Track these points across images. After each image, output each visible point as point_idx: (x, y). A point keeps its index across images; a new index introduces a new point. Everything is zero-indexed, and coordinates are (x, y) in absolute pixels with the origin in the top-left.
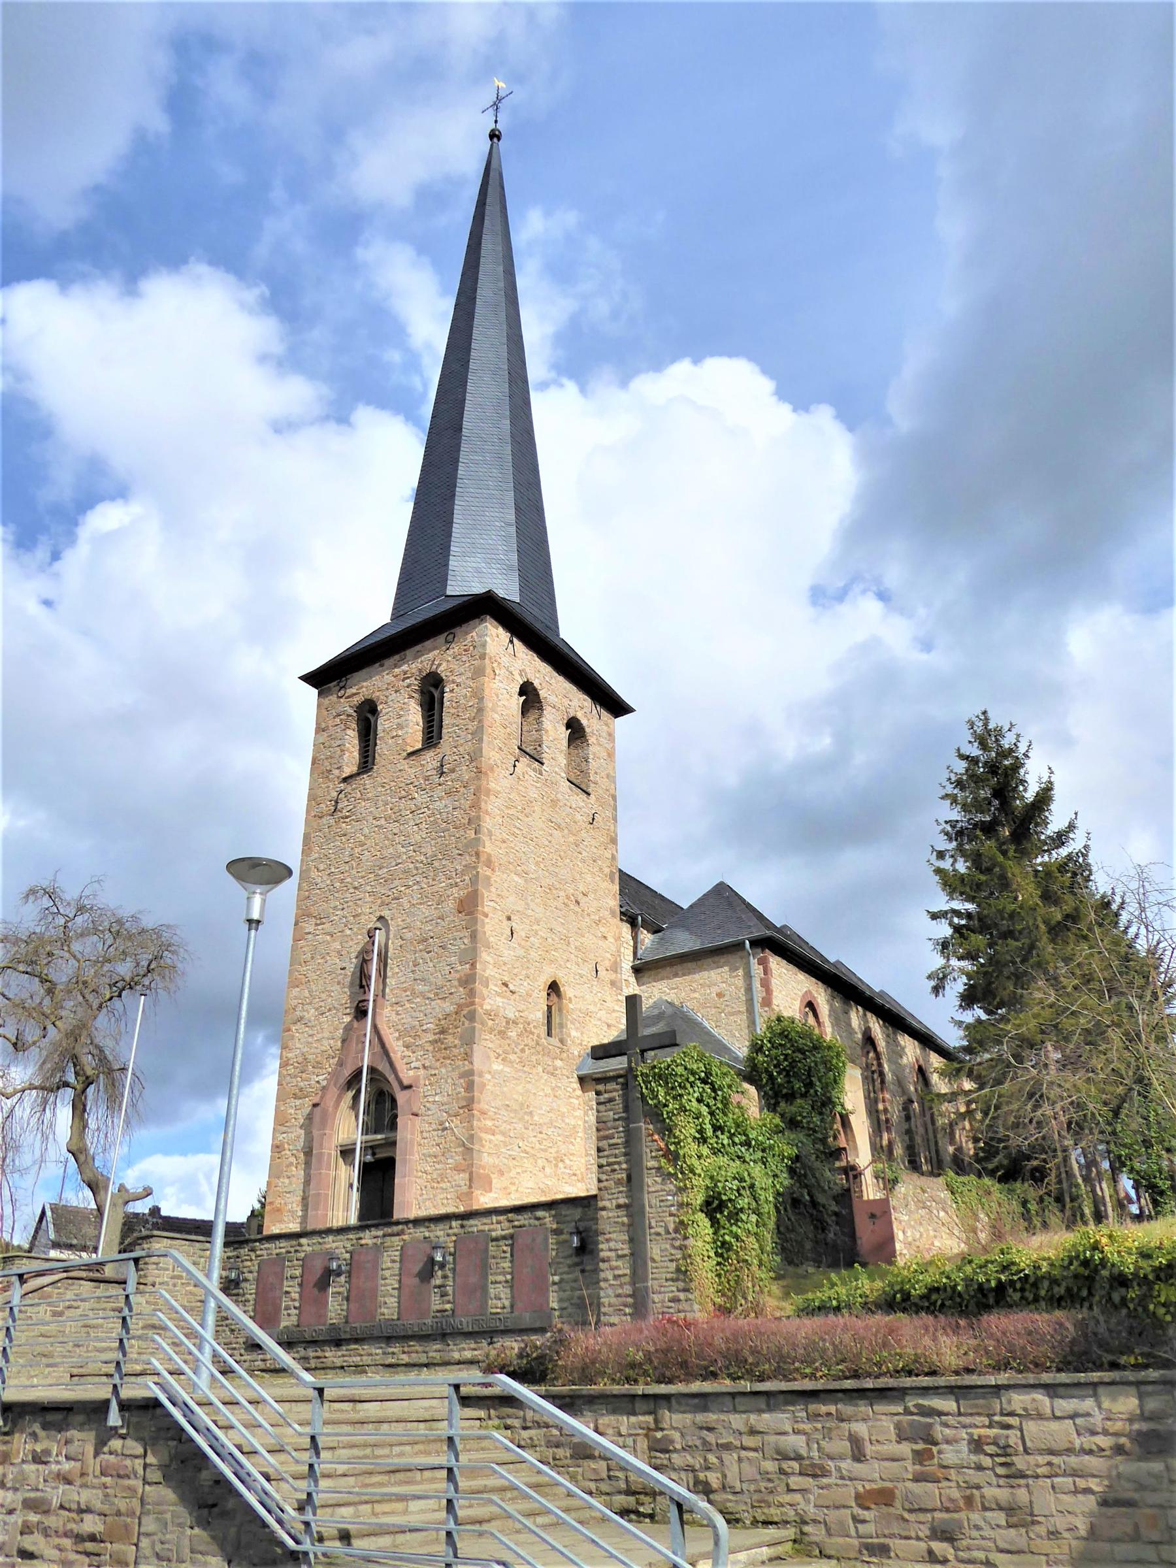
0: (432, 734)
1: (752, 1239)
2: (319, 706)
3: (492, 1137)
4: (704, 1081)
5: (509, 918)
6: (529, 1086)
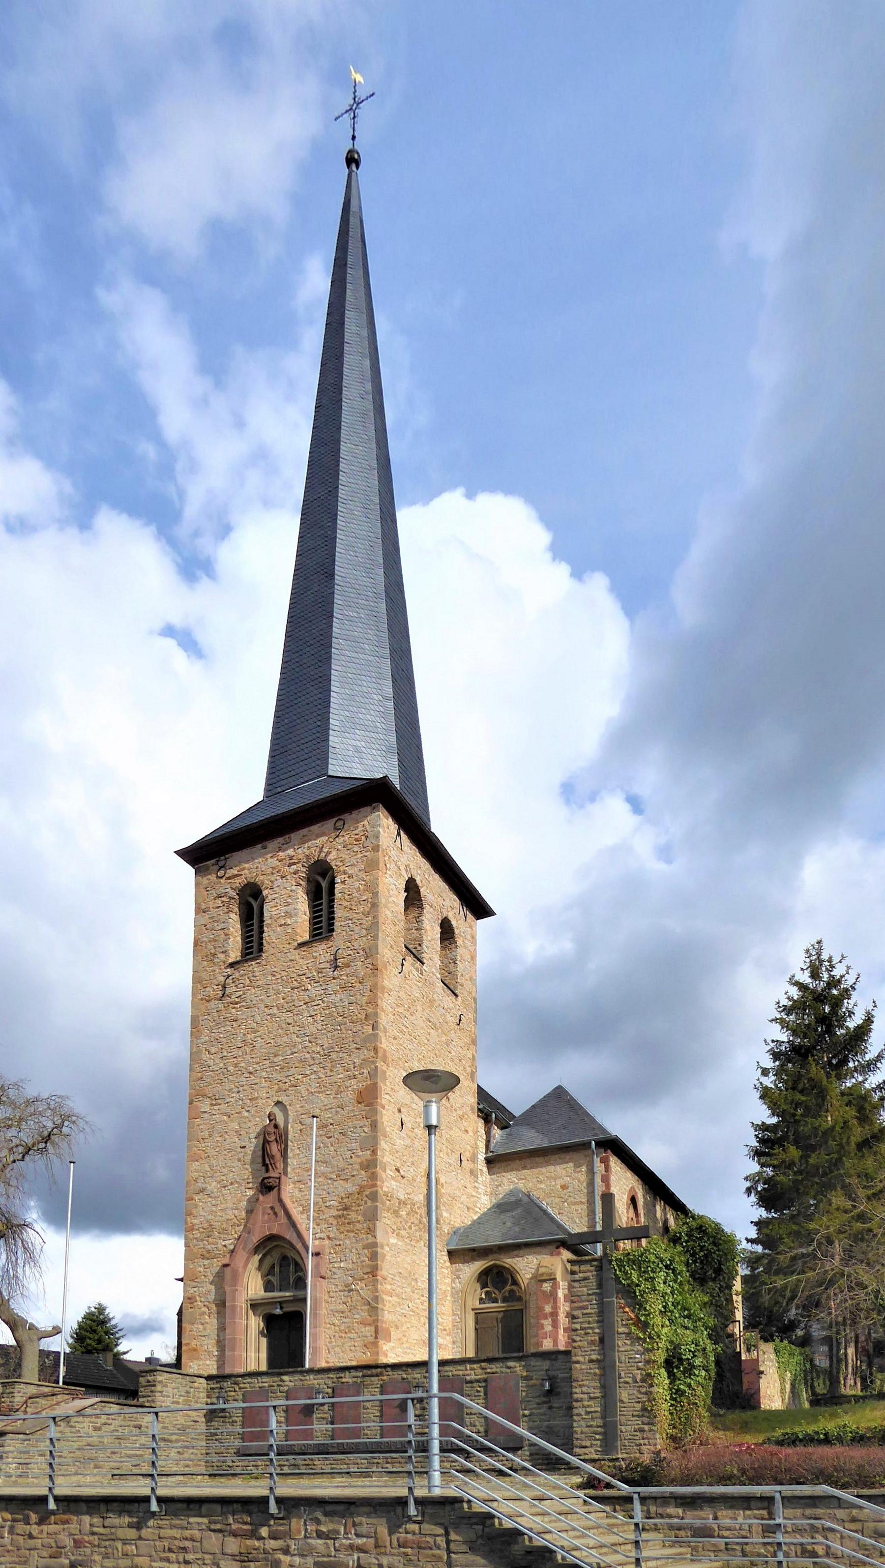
0: (322, 925)
2: (197, 885)
4: (667, 1267)
5: (400, 1111)
6: (415, 1257)
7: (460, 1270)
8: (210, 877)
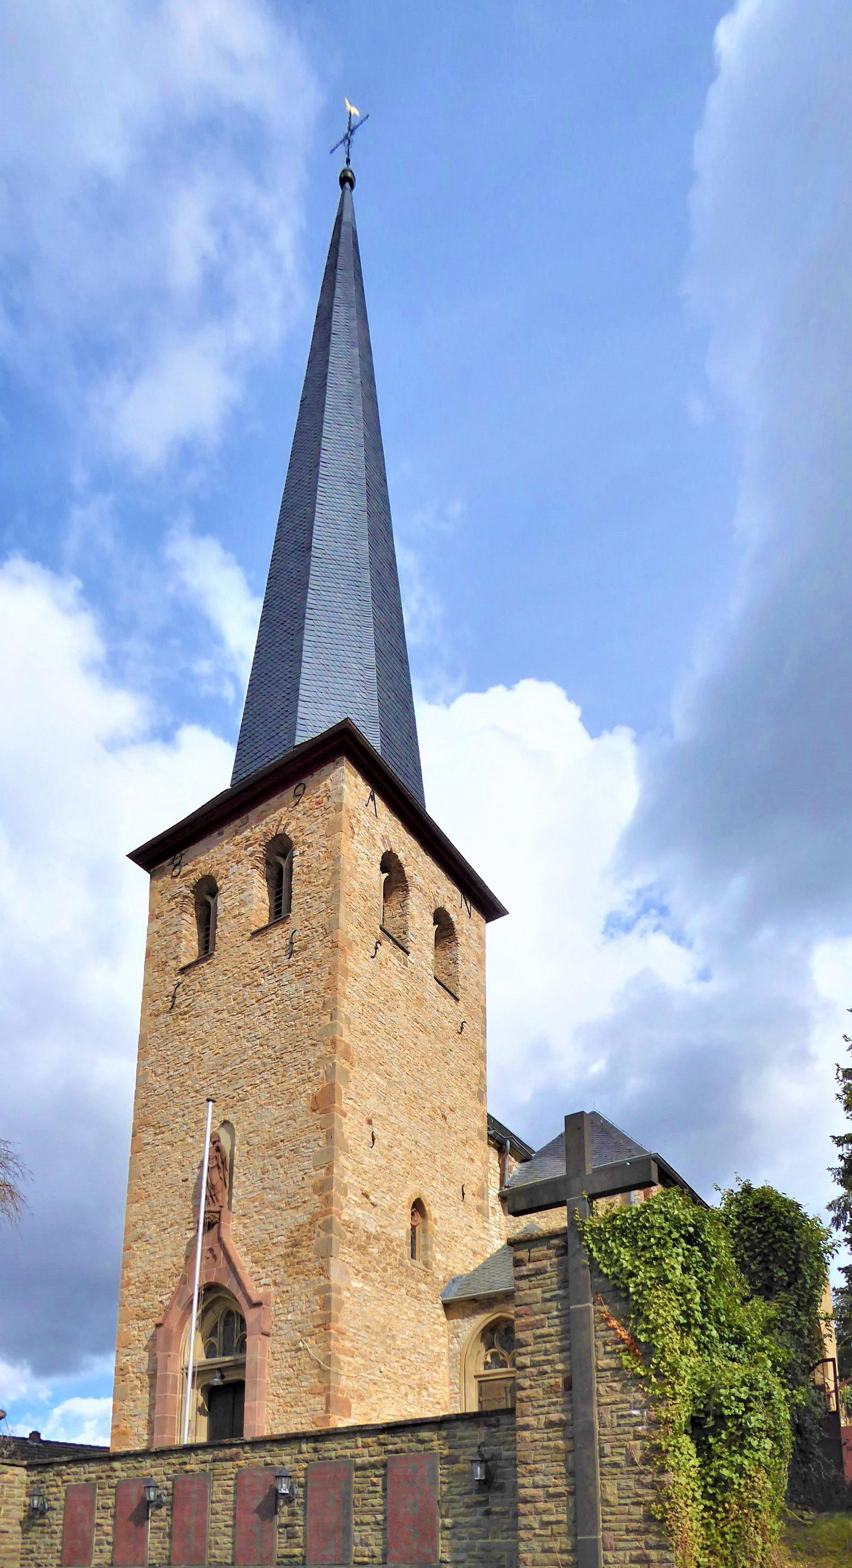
1: (762, 1474)
2: (152, 889)
3: (351, 1360)
4: (690, 1239)
5: (370, 1122)
7: (459, 1327)
8: (165, 878)
